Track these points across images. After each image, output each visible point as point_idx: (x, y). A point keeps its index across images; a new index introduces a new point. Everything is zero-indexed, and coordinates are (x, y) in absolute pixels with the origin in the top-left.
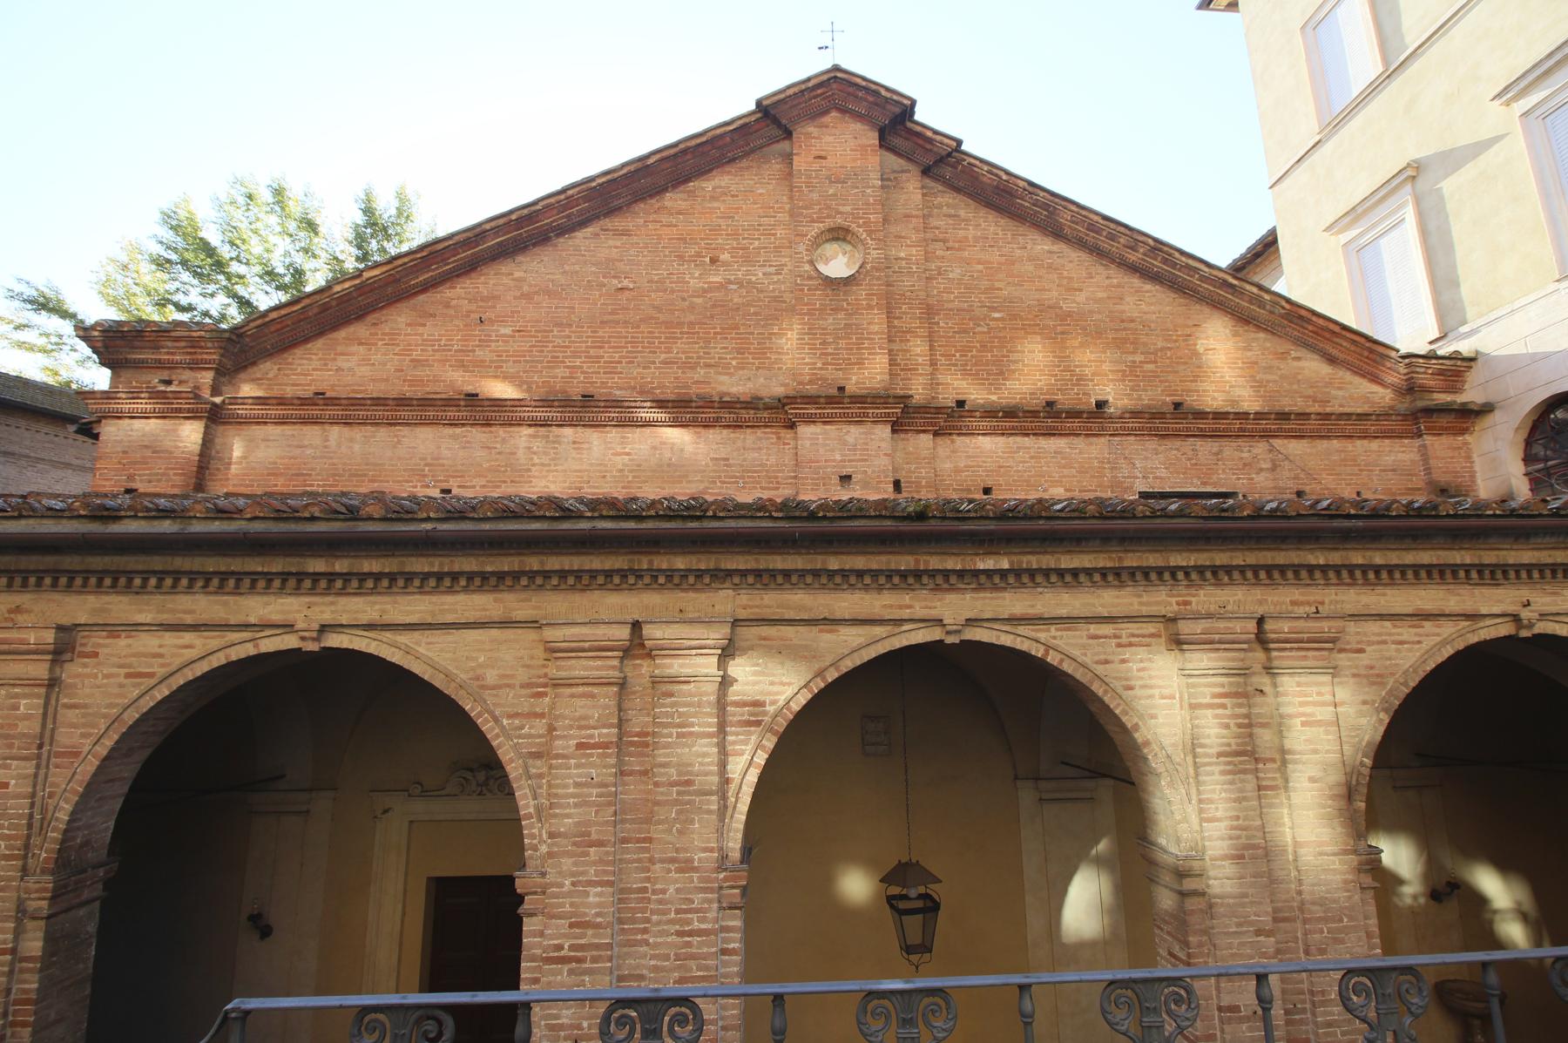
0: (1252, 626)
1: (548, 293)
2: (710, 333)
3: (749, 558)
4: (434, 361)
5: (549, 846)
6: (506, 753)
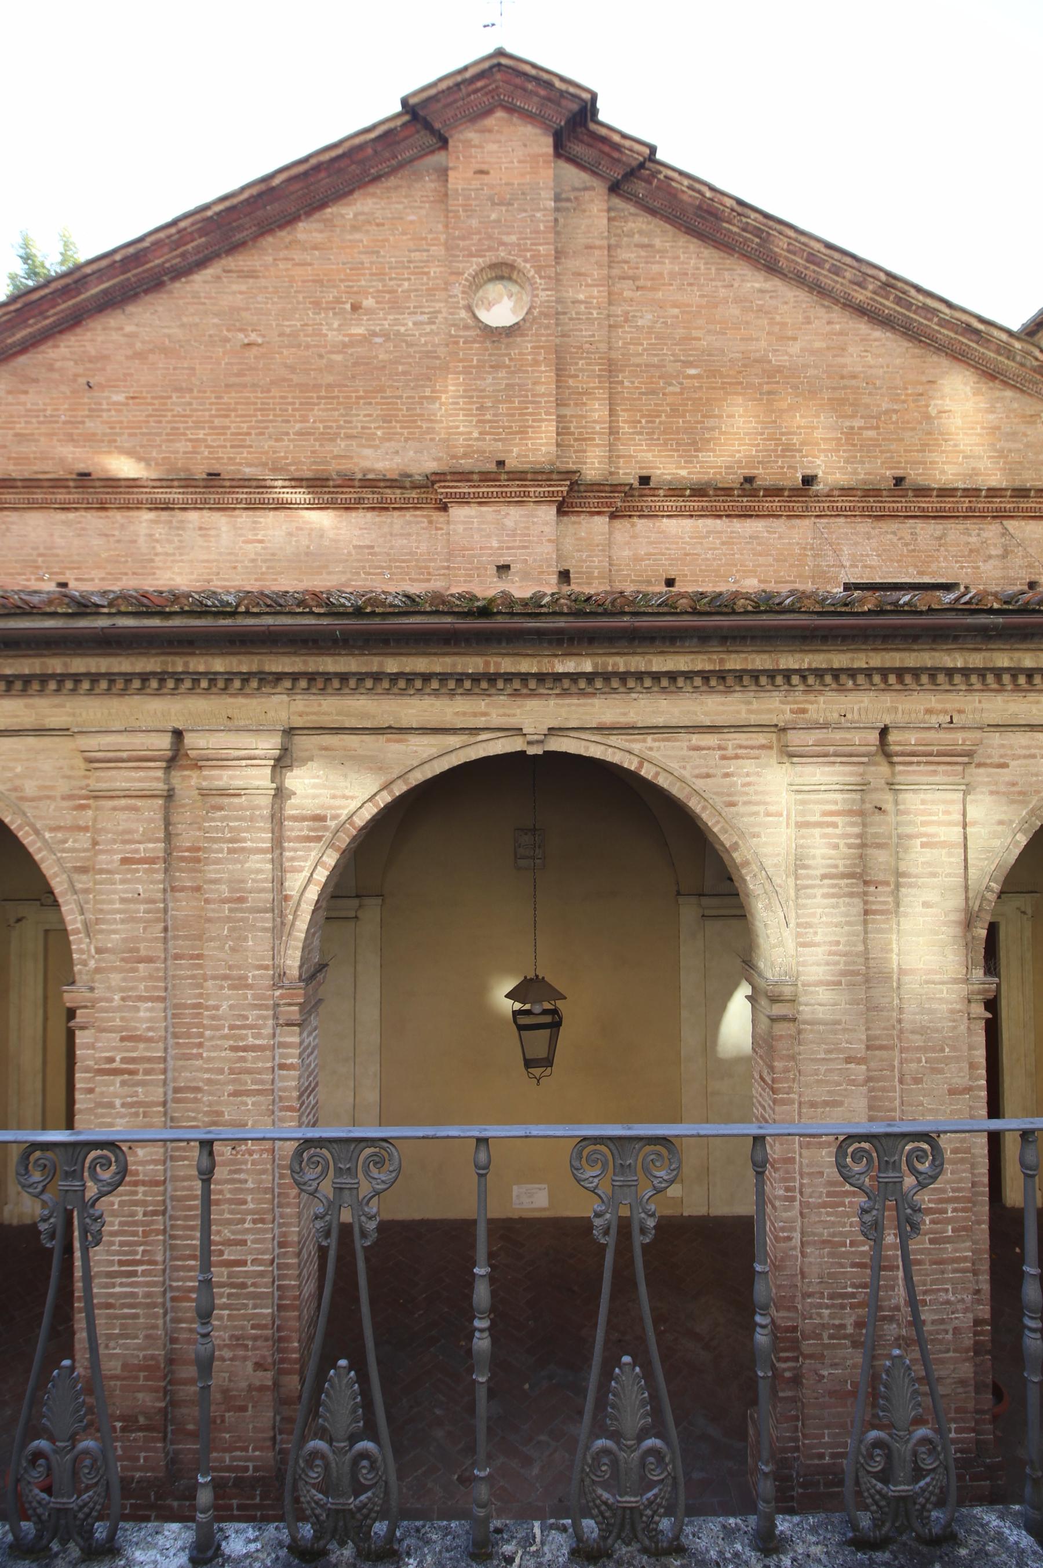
0: (874, 737)
1: (165, 351)
2: (350, 397)
3: (297, 659)
4: (40, 434)
5: (97, 961)
6: (49, 867)
